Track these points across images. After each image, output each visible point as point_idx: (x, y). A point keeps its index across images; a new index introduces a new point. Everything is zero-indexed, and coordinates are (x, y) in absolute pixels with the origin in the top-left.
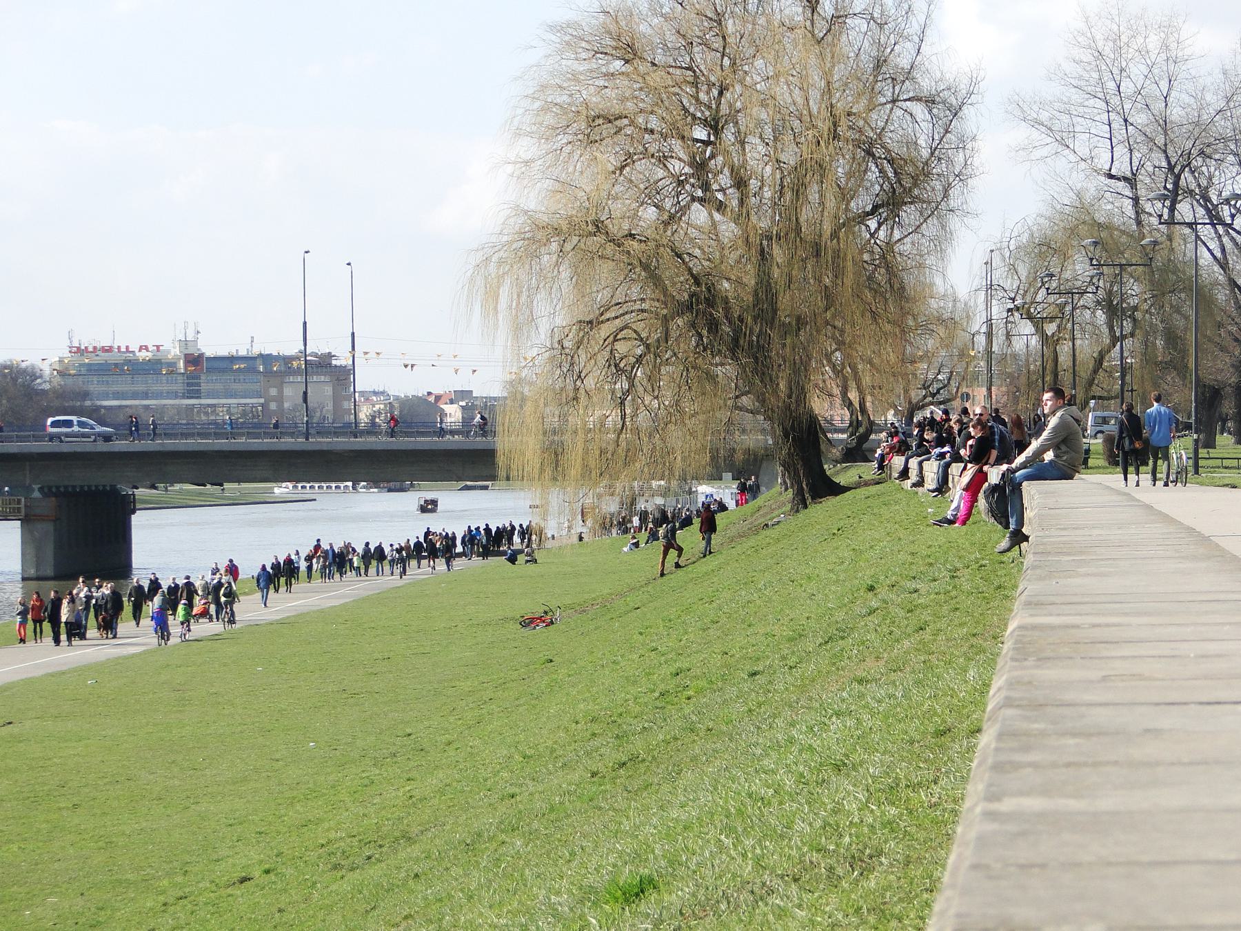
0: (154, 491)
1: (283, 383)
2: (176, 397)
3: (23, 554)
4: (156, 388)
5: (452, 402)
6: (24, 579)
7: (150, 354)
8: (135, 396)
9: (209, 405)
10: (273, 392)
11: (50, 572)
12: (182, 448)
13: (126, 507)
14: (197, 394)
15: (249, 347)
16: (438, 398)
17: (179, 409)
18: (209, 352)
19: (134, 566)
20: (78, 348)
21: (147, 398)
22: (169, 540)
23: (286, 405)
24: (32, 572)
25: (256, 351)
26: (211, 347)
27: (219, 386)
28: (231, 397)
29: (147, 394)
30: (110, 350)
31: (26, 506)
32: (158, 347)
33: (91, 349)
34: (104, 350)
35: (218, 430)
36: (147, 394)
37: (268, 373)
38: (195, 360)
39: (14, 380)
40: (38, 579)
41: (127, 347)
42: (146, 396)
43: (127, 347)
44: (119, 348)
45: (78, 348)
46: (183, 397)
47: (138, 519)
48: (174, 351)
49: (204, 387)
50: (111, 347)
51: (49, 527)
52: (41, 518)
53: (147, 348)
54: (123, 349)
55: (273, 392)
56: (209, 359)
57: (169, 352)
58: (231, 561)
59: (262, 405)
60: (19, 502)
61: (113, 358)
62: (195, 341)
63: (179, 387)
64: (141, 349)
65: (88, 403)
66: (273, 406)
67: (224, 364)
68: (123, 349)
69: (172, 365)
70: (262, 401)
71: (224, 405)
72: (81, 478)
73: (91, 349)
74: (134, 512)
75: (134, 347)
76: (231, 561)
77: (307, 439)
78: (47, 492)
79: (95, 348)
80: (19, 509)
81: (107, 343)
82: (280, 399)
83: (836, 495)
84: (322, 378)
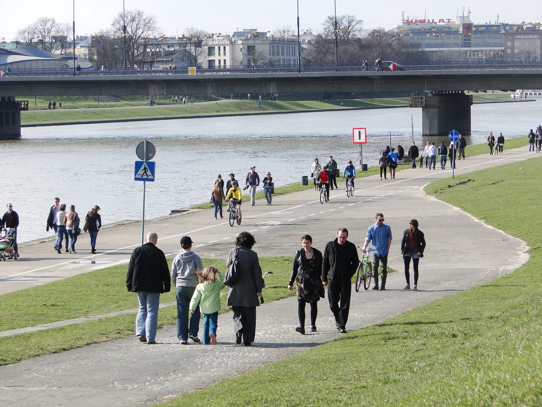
0: (485, 93)
1: (514, 39)
2: (458, 46)
3: (423, 124)
4: (447, 41)
6: (423, 135)
8: (436, 46)
9: (475, 51)
10: (509, 44)
11: (436, 132)
12: (41, 80)
13: (468, 102)
14: (468, 45)
15: (496, 20)
17: (460, 53)
18: (475, 22)
19: (472, 129)
20: (407, 21)
21: (443, 47)
22: (487, 117)
23: (516, 51)
24: (427, 132)
25: (501, 21)
26: (477, 20)
27: (481, 41)
28: (487, 46)
29: (443, 45)
30: (424, 21)
31: (425, 100)
32: (449, 20)
34: (421, 21)
35: (479, 64)
36: (443, 45)
37: (507, 34)
38: (468, 27)
39: (381, 38)
40: (430, 135)
41: (433, 20)
42: (442, 46)
43: (433, 20)
44: (429, 20)
45: (407, 21)
46: (462, 47)
47: (473, 108)
48: (457, 22)
49: (473, 41)
50: (425, 20)
51: (436, 110)
52: (432, 106)
53: (443, 21)
54: (431, 21)
55: (509, 44)
56: (475, 26)
57: (454, 22)
58: (415, 223)
59: (503, 51)
60: (422, 98)
61: (426, 26)
62: (469, 17)
63: (460, 41)
65: (420, 50)
66: (509, 51)
67: (488, 30)
68: (431, 21)
70: (503, 48)
71: (482, 50)
72: (451, 88)
74: (472, 104)
76: (415, 223)
78: (439, 94)
79: (416, 20)
80: (422, 102)
81: (422, 18)
82: (512, 48)
84: (535, 37)
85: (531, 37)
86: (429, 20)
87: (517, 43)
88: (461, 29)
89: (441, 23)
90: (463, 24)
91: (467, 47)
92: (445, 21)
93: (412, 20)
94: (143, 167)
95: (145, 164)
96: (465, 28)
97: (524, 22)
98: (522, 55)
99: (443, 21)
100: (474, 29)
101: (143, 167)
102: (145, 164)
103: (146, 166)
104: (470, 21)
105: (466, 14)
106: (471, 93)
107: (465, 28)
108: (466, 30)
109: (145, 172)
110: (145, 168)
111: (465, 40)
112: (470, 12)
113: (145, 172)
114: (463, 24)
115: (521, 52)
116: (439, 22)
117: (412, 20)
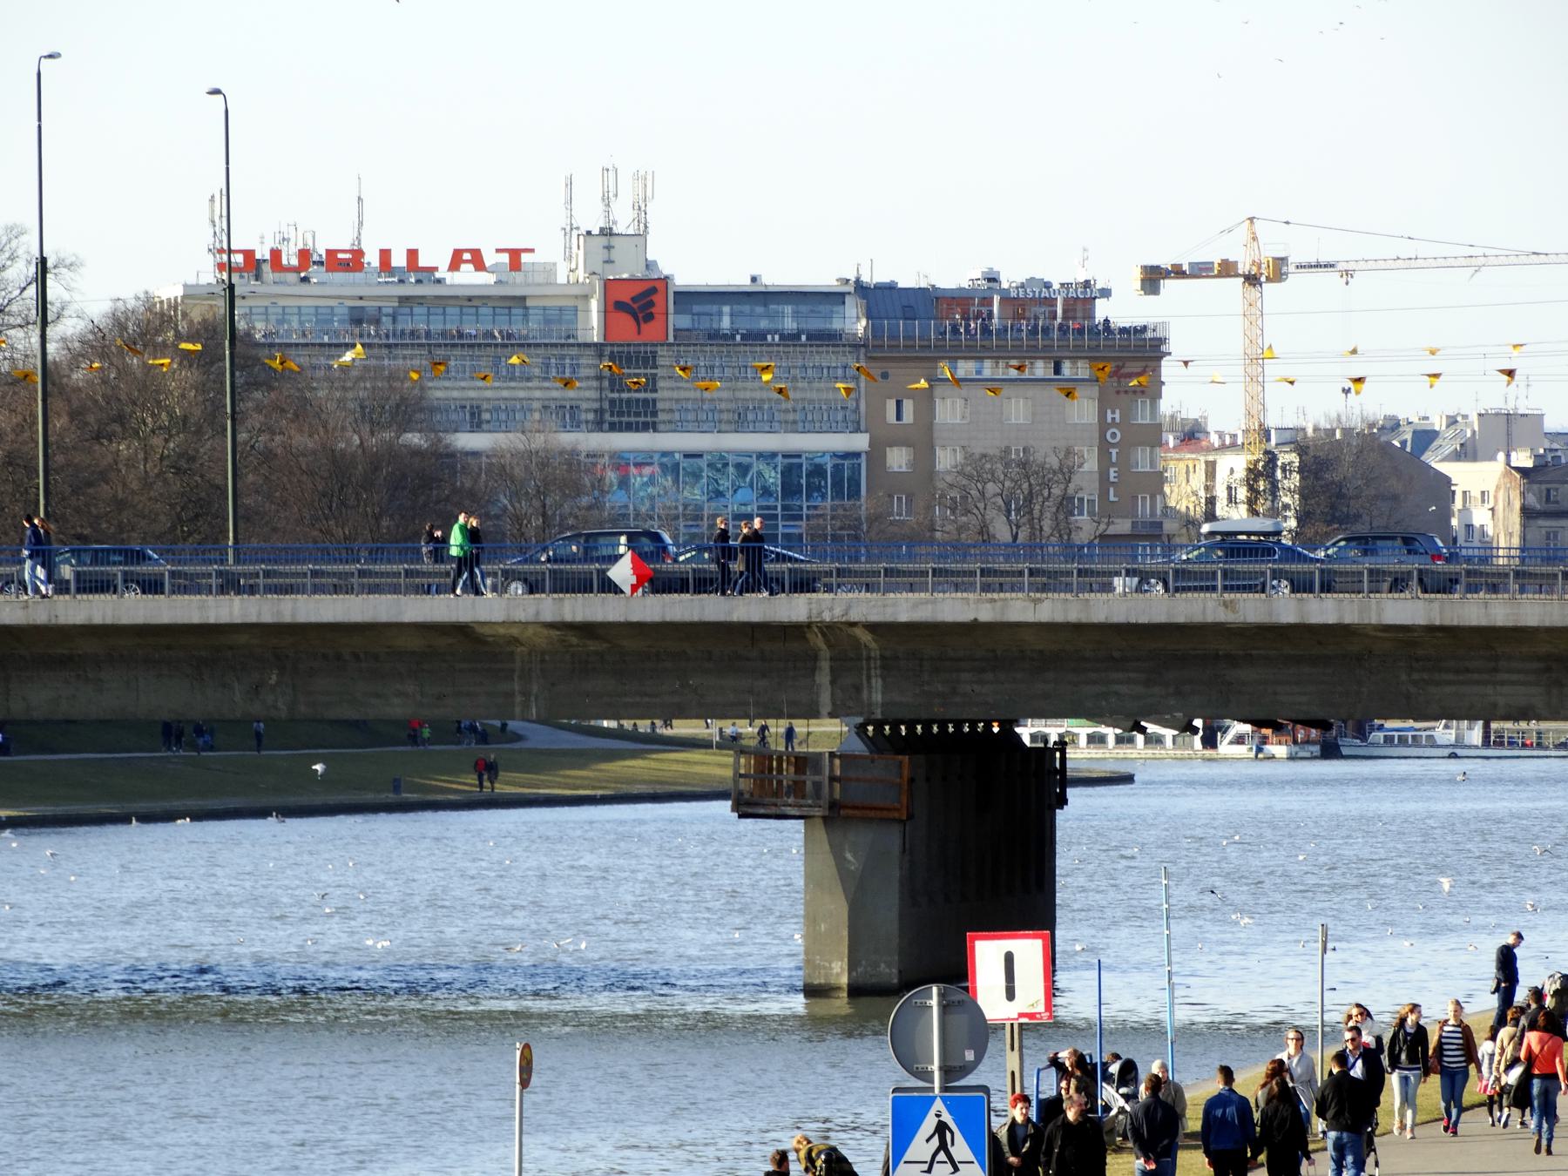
3: (901, 916)
5: (1466, 452)
7: (486, 278)
13: (1046, 779)
14: (641, 416)
16: (1426, 438)
23: (946, 460)
26: (693, 258)
30: (352, 262)
32: (515, 254)
33: (290, 258)
34: (333, 261)
38: (640, 300)
41: (413, 254)
43: (413, 254)
44: (385, 255)
46: (599, 425)
48: (561, 264)
51: (892, 839)
53: (478, 261)
54: (399, 260)
56: (688, 298)
57: (550, 269)
62: (641, 236)
63: (585, 394)
64: (456, 261)
68: (399, 260)
69: (566, 312)
72: (967, 701)
73: (290, 258)
75: (435, 257)
77: (504, 725)
79: (304, 255)
81: (342, 241)
82: (923, 441)
83: (844, 1160)
85: (988, 369)
86: (385, 255)
87: (949, 411)
88: (592, 324)
89: (467, 277)
90: (608, 285)
91: (629, 428)
92: (490, 259)
93: (276, 254)
94: (929, 1124)
95: (938, 1105)
96: (620, 306)
97: (992, 279)
98: (991, 488)
99: (479, 264)
100: (676, 321)
101: (929, 1124)
102: (938, 1105)
103: (947, 1118)
104: (649, 265)
105: (624, 223)
106: (1053, 730)
107: (620, 306)
108: (625, 321)
109: (943, 1146)
110: (941, 1128)
111: (616, 383)
112: (1348, 274)
113: (943, 1146)
114: (608, 285)
115: (976, 468)
116: (455, 264)
117: (276, 254)
